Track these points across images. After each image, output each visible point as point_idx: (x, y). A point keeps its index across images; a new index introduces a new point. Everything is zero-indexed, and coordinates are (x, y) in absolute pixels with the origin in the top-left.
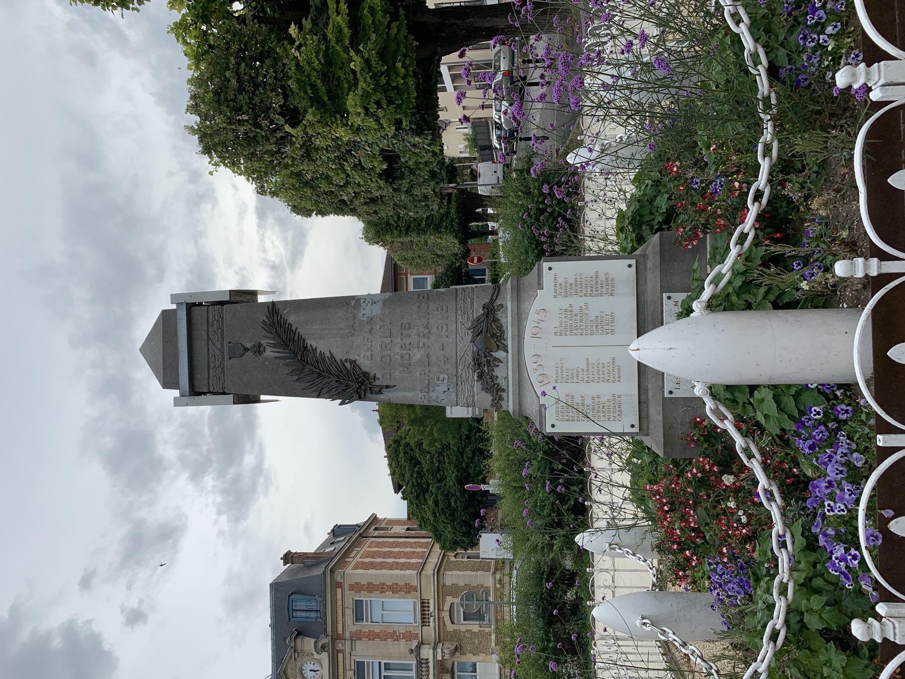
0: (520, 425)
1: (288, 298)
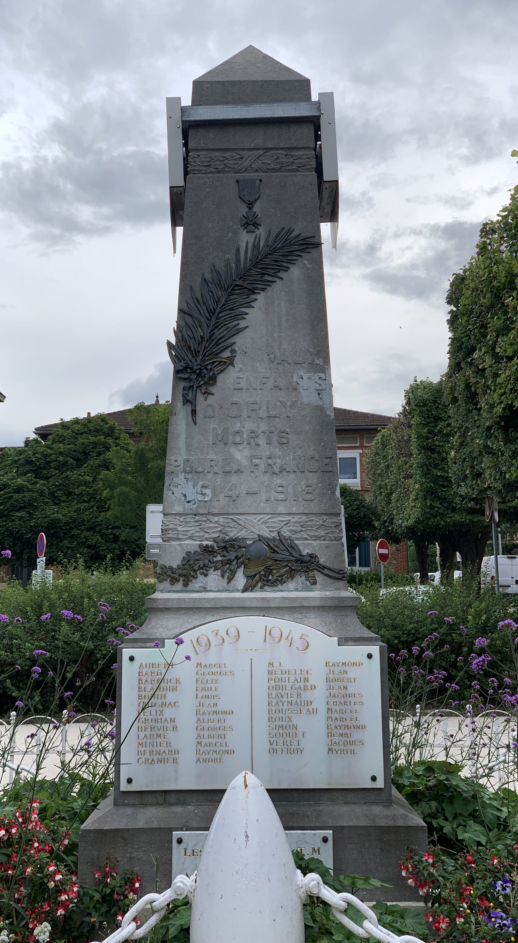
0: (136, 610)
1: (327, 269)
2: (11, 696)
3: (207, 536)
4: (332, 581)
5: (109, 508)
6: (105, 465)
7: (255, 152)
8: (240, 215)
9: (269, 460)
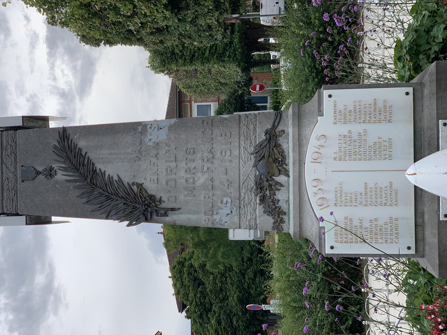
1: (77, 124)
2: (351, 325)
3: (253, 200)
4: (282, 120)
5: (230, 265)
6: (202, 267)
7: (4, 170)
8: (45, 179)
9: (205, 160)
